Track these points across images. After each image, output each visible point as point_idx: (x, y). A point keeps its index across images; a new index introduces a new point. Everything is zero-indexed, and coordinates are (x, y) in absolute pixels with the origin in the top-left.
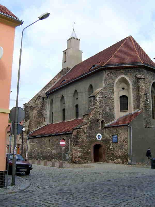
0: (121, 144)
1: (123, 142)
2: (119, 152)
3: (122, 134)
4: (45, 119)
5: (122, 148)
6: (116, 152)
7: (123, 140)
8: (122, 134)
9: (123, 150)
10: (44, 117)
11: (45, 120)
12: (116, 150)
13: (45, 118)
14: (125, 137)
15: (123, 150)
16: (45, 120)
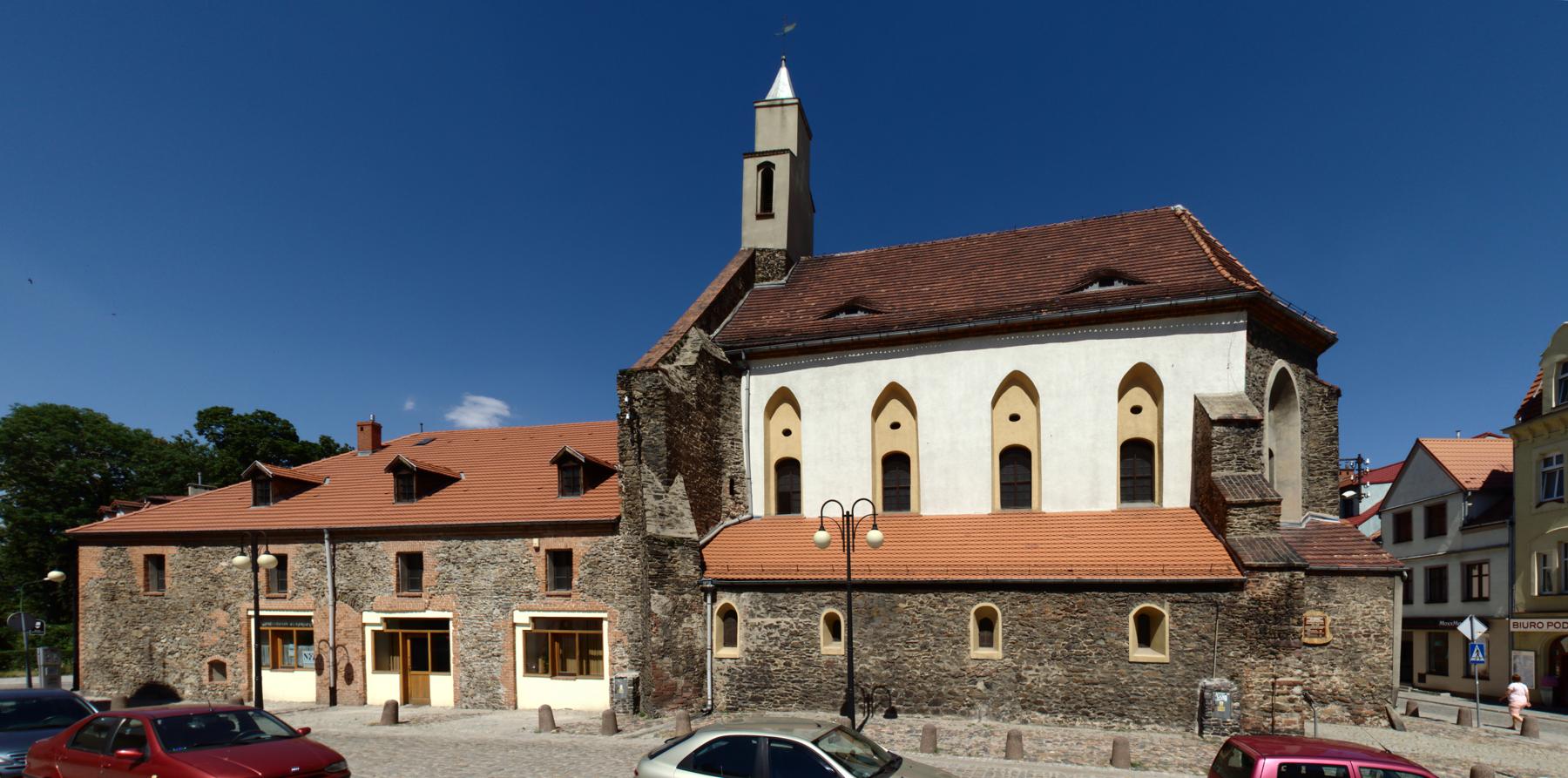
0: (1349, 643)
1: (1366, 639)
2: (1334, 678)
3: (1353, 605)
4: (736, 488)
5: (1357, 662)
6: (1319, 675)
7: (1363, 631)
8: (1353, 605)
9: (1356, 669)
10: (728, 474)
11: (732, 492)
12: (1317, 667)
13: (732, 483)
14: (1373, 618)
15: (1356, 669)
16: (732, 492)
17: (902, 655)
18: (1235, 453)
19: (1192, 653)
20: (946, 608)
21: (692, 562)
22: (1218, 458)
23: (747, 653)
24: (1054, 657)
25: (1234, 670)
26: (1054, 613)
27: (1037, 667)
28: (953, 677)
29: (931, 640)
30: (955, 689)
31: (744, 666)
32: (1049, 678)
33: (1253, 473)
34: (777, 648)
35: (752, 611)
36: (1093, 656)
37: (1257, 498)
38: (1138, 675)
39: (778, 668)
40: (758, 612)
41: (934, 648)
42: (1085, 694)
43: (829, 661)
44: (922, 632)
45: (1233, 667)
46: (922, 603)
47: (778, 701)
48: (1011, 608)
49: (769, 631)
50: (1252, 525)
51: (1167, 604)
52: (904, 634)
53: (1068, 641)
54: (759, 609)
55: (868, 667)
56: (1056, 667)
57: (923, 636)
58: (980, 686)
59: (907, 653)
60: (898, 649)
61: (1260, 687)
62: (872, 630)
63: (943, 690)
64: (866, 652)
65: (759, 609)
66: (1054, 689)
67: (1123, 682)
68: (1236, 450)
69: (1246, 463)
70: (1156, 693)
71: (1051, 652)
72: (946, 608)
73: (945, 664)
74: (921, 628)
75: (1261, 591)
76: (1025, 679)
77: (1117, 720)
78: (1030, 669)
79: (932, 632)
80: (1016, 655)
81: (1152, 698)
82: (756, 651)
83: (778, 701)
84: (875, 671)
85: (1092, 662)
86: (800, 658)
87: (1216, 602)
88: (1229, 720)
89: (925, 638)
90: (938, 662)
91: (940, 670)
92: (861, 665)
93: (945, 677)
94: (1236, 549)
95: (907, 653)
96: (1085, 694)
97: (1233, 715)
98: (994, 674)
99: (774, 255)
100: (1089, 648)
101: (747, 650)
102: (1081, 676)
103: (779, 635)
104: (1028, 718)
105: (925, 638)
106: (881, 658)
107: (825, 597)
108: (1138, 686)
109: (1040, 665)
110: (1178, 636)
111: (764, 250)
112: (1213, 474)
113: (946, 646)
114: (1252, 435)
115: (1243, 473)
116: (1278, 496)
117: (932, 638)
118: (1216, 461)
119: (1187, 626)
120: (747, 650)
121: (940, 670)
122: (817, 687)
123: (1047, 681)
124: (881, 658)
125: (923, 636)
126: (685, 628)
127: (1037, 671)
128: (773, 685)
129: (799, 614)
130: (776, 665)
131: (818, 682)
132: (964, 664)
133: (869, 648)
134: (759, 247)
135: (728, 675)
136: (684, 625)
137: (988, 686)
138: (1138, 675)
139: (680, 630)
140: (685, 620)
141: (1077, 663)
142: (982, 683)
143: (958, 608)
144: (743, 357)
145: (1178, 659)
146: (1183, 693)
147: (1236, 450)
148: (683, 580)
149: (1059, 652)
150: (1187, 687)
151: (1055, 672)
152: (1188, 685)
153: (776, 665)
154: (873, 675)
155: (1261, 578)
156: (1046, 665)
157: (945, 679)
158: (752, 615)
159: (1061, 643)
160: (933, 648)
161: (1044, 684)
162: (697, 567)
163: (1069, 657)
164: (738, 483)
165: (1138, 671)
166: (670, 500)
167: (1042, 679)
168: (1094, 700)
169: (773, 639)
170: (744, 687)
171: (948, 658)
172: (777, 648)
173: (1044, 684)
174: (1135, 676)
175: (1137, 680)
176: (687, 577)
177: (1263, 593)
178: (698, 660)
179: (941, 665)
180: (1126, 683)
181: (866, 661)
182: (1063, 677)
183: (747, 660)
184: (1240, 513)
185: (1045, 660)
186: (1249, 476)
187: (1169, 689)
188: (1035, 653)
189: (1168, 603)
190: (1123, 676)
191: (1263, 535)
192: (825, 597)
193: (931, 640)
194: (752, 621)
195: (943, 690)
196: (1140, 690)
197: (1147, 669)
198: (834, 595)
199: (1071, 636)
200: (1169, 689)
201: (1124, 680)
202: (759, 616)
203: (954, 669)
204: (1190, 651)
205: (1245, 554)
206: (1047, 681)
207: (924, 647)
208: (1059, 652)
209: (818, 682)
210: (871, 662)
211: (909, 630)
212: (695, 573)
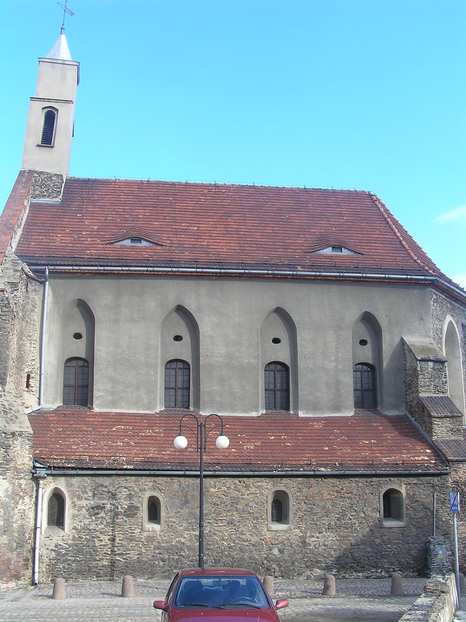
10: (26, 370)
13: (29, 377)
17: (212, 530)
18: (432, 381)
19: (420, 520)
20: (248, 492)
21: (27, 452)
22: (422, 384)
23: (74, 531)
24: (329, 528)
25: (445, 530)
26: (329, 494)
27: (318, 535)
28: (253, 545)
29: (236, 517)
30: (255, 555)
31: (70, 542)
32: (326, 543)
33: (443, 395)
34: (103, 526)
35: (79, 495)
36: (357, 525)
37: (449, 414)
38: (388, 537)
39: (103, 543)
40: (86, 496)
41: (238, 524)
42: (351, 553)
43: (149, 536)
44: (228, 511)
45: (445, 528)
46: (229, 488)
47: (101, 572)
48: (298, 491)
49: (96, 511)
50: (447, 431)
51: (404, 486)
52: (214, 513)
53: (339, 514)
54: (86, 493)
55: (183, 540)
56: (332, 534)
57: (230, 514)
58: (275, 551)
59: (216, 528)
60: (209, 525)
61: (461, 541)
62: (187, 510)
63: (245, 557)
64: (182, 528)
65: (86, 493)
66: (330, 550)
67: (377, 543)
68: (432, 379)
69: (439, 388)
70: (399, 549)
71: (327, 524)
72: (248, 492)
73: (248, 536)
74: (228, 508)
75: (458, 476)
76: (310, 545)
77: (374, 571)
78: (313, 537)
79: (237, 511)
80: (302, 527)
81: (396, 553)
82: (83, 529)
83: (101, 572)
84: (188, 544)
85: (356, 529)
86: (123, 534)
87: (433, 484)
88: (446, 564)
89: (232, 515)
90: (242, 534)
91: (244, 541)
92: (177, 539)
93: (247, 546)
94: (440, 448)
95: (216, 528)
96: (351, 553)
97: (448, 560)
98: (286, 542)
99: (51, 177)
100: (354, 519)
101: (75, 528)
102: (348, 540)
103: (104, 515)
104: (312, 573)
105: (232, 515)
106: (194, 533)
107: (147, 483)
108: (387, 544)
109: (319, 533)
110: (411, 508)
111: (42, 173)
112: (420, 395)
113: (248, 521)
114: (441, 370)
115: (437, 395)
116: (461, 413)
117: (237, 516)
118: (421, 386)
119: (417, 501)
120: (75, 528)
121: (244, 541)
122: (138, 558)
123: (325, 546)
124: (194, 533)
125: (230, 514)
126: (20, 510)
127: (317, 538)
128: (97, 558)
129: (123, 497)
130: (101, 540)
131: (139, 554)
132: (263, 536)
133: (184, 525)
134: (37, 170)
135: (54, 551)
136: (19, 507)
137: (281, 551)
138: (388, 537)
139: (16, 511)
140: (20, 502)
141: (346, 531)
142: (277, 549)
143: (258, 492)
144: (47, 273)
145: (412, 524)
146: (416, 547)
147: (432, 379)
148: (21, 467)
149: (333, 523)
150: (418, 544)
151: (330, 538)
152: (419, 542)
153: (101, 540)
154: (188, 547)
155: (457, 468)
156: (324, 533)
157: (247, 548)
158: (80, 498)
159: (334, 516)
160: (237, 524)
161: (323, 547)
162: (31, 456)
163: (339, 527)
164: (33, 378)
165: (386, 534)
166: (8, 398)
167: (321, 544)
168: (358, 557)
169: (99, 518)
170: (69, 560)
171: (250, 531)
172: (103, 526)
173: (323, 547)
174: (385, 538)
175: (386, 540)
176: (23, 464)
177: (459, 478)
178: (27, 537)
179: (244, 537)
180: (379, 543)
181: (182, 536)
182: (336, 541)
183: (74, 537)
184: (440, 423)
185: (323, 529)
186: (441, 397)
187: (407, 546)
188: (316, 525)
189: (405, 486)
190: (377, 538)
191: (453, 438)
192: (147, 483)
193: (236, 517)
194: (78, 503)
195: (245, 557)
196: (388, 547)
197: (393, 532)
198: (155, 481)
199: (341, 511)
200: (407, 546)
201: (378, 541)
202: (86, 499)
203: (255, 539)
204: (419, 518)
205: (447, 452)
206: (325, 546)
207: (231, 523)
208: (333, 523)
209: (139, 554)
210: (186, 536)
211: (218, 509)
212: (29, 461)
